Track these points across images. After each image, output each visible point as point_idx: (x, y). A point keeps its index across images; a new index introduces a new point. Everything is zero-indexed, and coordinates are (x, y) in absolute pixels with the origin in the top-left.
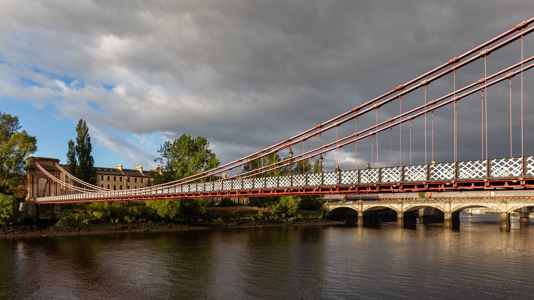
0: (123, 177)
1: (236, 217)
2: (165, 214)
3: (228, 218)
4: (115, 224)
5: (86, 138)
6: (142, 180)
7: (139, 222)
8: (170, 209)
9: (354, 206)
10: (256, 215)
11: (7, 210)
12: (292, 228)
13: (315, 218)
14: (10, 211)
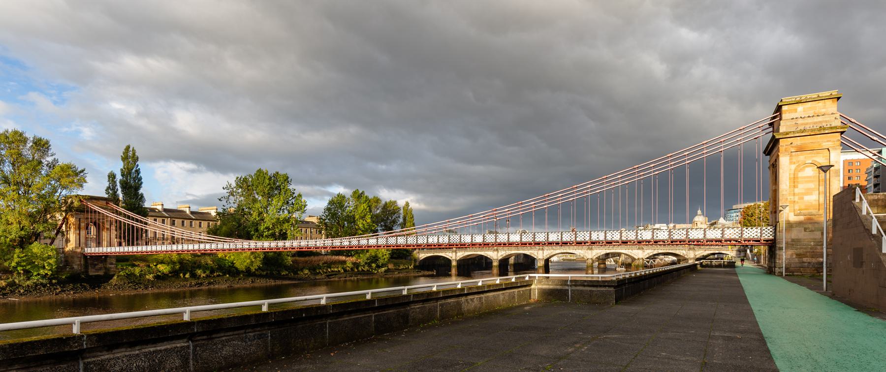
0: (166, 219)
1: (324, 268)
2: (246, 266)
3: (314, 269)
4: (186, 280)
5: (135, 169)
6: (191, 222)
7: (214, 276)
8: (253, 260)
9: (447, 254)
10: (345, 266)
11: (49, 264)
12: (383, 279)
13: (406, 268)
14: (52, 265)
